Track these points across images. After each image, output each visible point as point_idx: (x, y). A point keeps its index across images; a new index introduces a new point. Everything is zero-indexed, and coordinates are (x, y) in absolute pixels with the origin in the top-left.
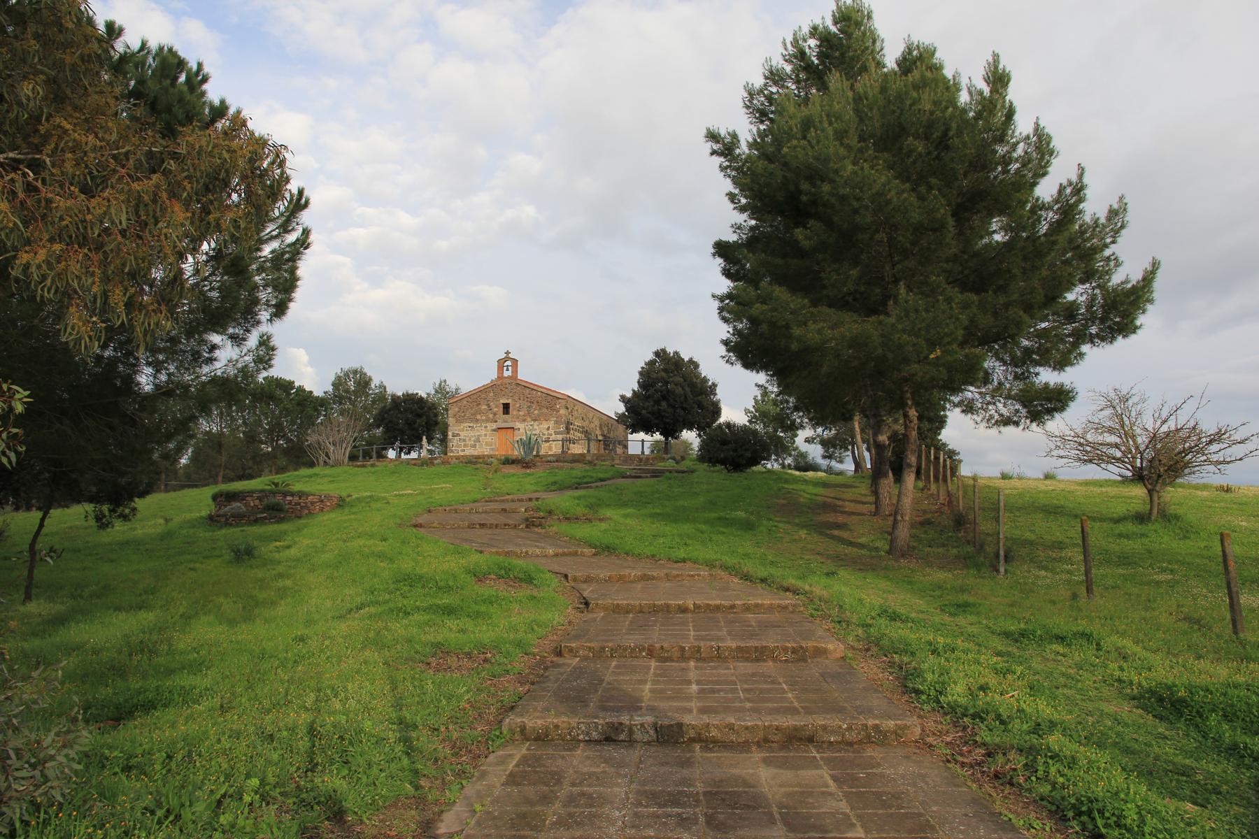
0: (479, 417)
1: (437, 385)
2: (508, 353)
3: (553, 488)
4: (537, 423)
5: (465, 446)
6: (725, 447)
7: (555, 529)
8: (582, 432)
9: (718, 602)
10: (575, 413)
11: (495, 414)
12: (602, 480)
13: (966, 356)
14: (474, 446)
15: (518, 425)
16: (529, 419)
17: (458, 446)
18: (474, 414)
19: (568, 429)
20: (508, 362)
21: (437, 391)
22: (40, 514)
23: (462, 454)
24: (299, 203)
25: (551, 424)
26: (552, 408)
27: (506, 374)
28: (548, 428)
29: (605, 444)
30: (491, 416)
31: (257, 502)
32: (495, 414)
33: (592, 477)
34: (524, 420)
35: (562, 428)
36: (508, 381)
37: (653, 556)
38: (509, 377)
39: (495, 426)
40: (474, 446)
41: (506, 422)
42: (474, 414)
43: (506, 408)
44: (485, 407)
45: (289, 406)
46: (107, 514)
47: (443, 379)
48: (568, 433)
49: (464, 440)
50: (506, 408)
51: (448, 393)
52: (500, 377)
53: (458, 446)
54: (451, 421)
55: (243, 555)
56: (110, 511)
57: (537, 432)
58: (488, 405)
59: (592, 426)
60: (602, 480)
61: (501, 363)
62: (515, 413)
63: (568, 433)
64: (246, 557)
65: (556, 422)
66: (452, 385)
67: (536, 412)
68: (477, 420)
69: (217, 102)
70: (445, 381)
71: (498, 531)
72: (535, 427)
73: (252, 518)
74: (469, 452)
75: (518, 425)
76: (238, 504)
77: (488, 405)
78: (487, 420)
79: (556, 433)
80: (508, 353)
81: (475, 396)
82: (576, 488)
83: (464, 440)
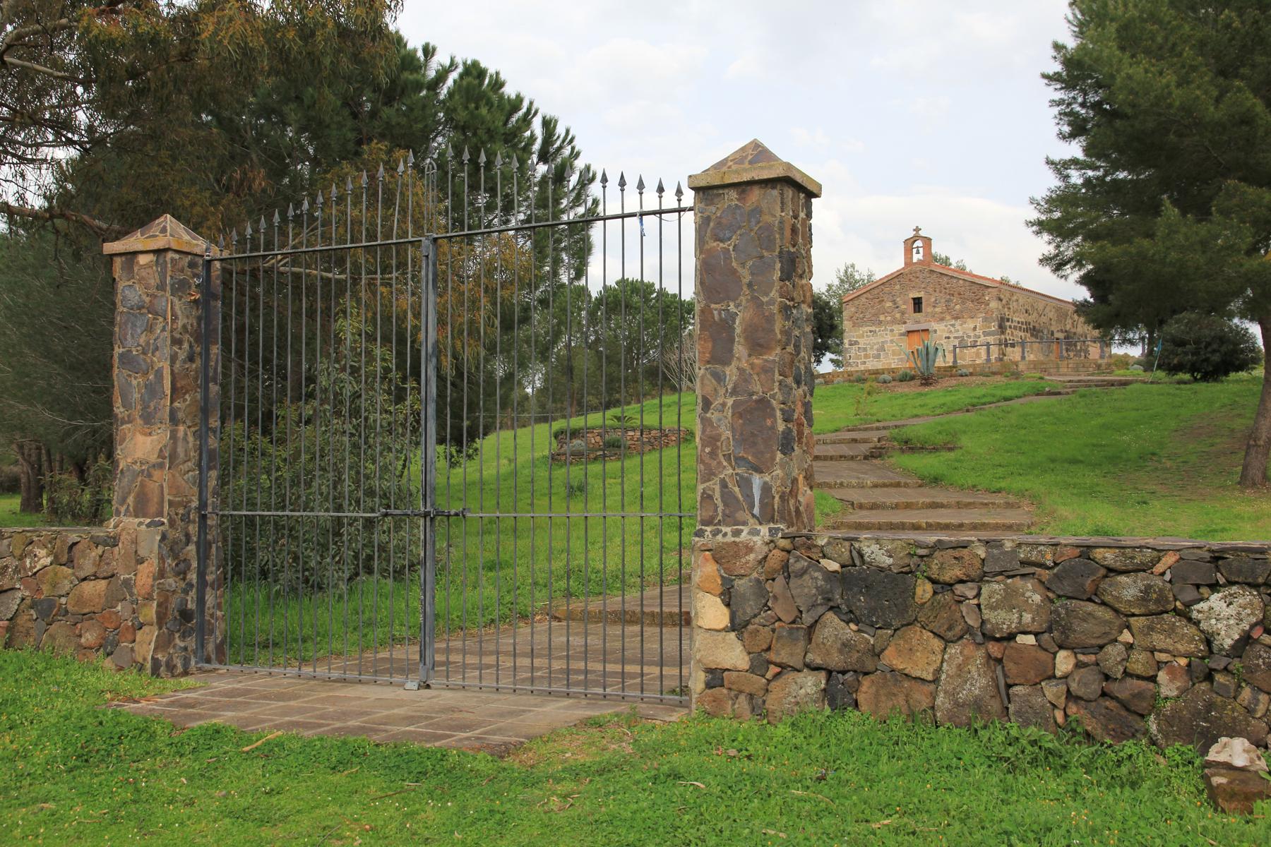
0: (882, 318)
1: (842, 274)
2: (917, 229)
3: (938, 411)
4: (959, 321)
5: (866, 356)
6: (1180, 350)
7: (893, 460)
8: (1026, 330)
9: (948, 521)
10: (1013, 305)
11: (903, 313)
12: (1006, 399)
13: (1259, 264)
14: (878, 356)
15: (934, 326)
16: (948, 317)
17: (858, 357)
18: (876, 315)
19: (1002, 328)
20: (917, 240)
21: (842, 281)
22: (513, 432)
23: (862, 368)
24: (587, 178)
25: (979, 322)
26: (978, 301)
27: (916, 257)
28: (975, 329)
29: (1067, 344)
30: (898, 316)
31: (598, 439)
32: (903, 313)
33: (994, 396)
34: (942, 319)
35: (994, 326)
36: (919, 268)
37: (974, 486)
38: (920, 262)
39: (903, 329)
40: (878, 356)
41: (918, 322)
42: (876, 315)
43: (917, 303)
44: (889, 304)
45: (649, 315)
46: (455, 454)
47: (849, 263)
48: (1003, 333)
49: (865, 349)
50: (917, 303)
51: (856, 282)
52: (909, 262)
53: (858, 357)
54: (847, 325)
55: (576, 490)
56: (457, 451)
57: (960, 334)
58: (894, 302)
59: (1044, 319)
60: (1006, 399)
61: (909, 245)
62: (930, 310)
63: (1003, 333)
64: (578, 493)
65: (985, 320)
66: (862, 272)
67: (958, 307)
68: (881, 322)
69: (513, 96)
70: (853, 266)
71: (828, 463)
72: (958, 327)
73: (592, 456)
74: (872, 365)
75: (934, 326)
76: (579, 442)
77: (894, 302)
78: (894, 321)
79: (986, 334)
80: (917, 229)
81: (876, 291)
82: (968, 411)
83: (865, 349)
